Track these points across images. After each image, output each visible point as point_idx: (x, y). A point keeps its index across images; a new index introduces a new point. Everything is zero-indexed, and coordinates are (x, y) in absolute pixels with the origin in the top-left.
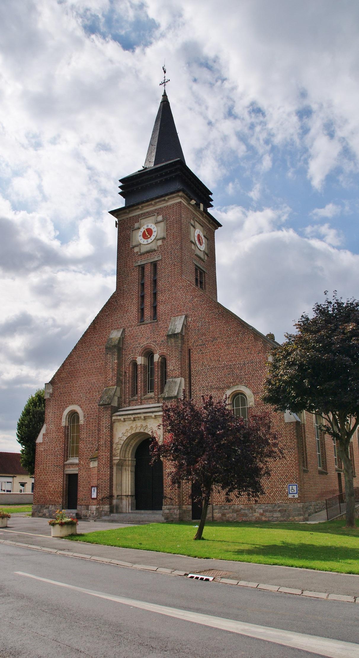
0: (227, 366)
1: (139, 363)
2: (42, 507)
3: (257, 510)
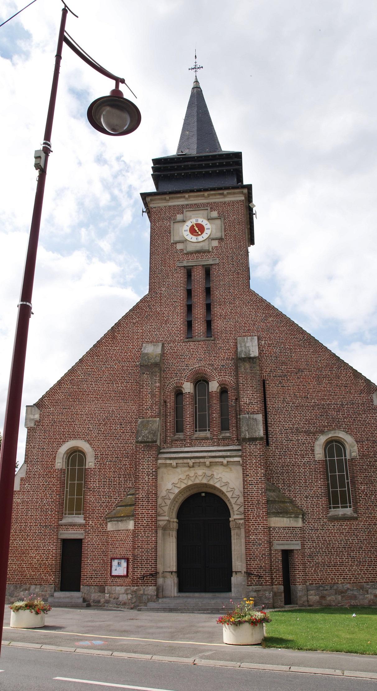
0: (318, 405)
2: (16, 587)
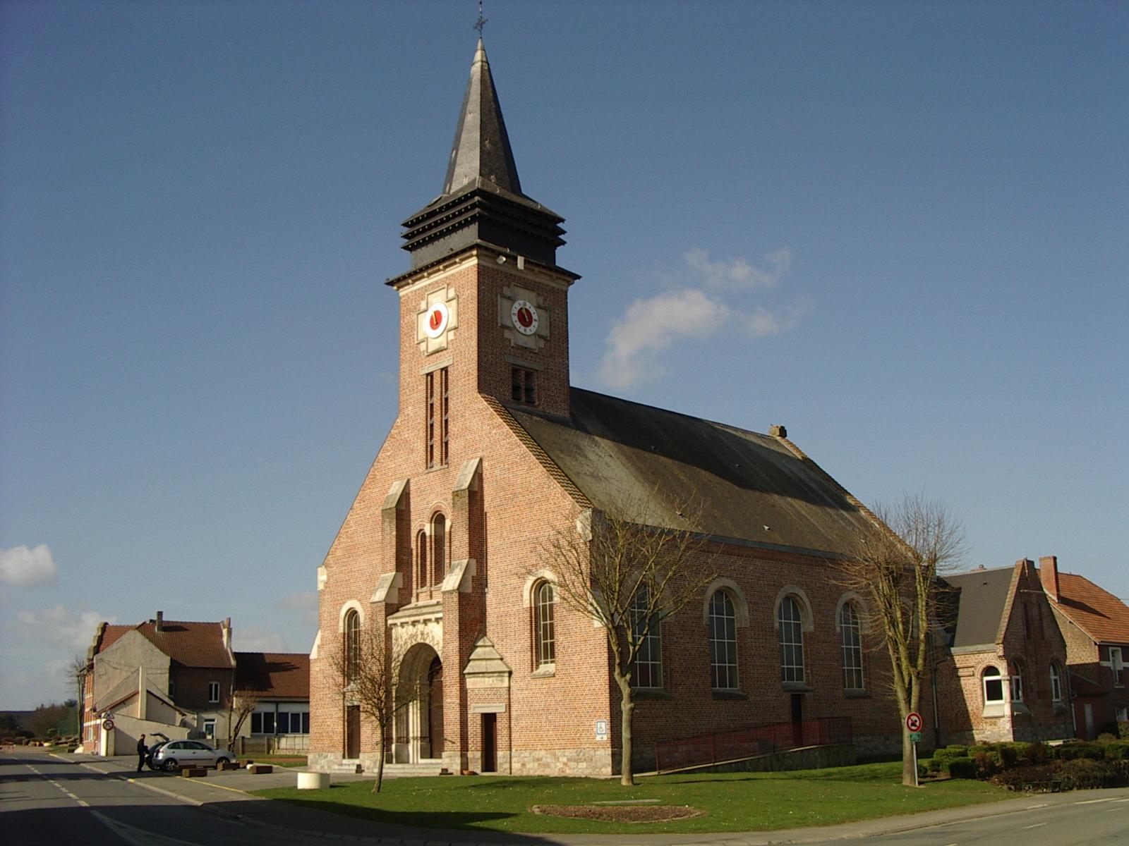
1: (428, 534)
3: (561, 759)
